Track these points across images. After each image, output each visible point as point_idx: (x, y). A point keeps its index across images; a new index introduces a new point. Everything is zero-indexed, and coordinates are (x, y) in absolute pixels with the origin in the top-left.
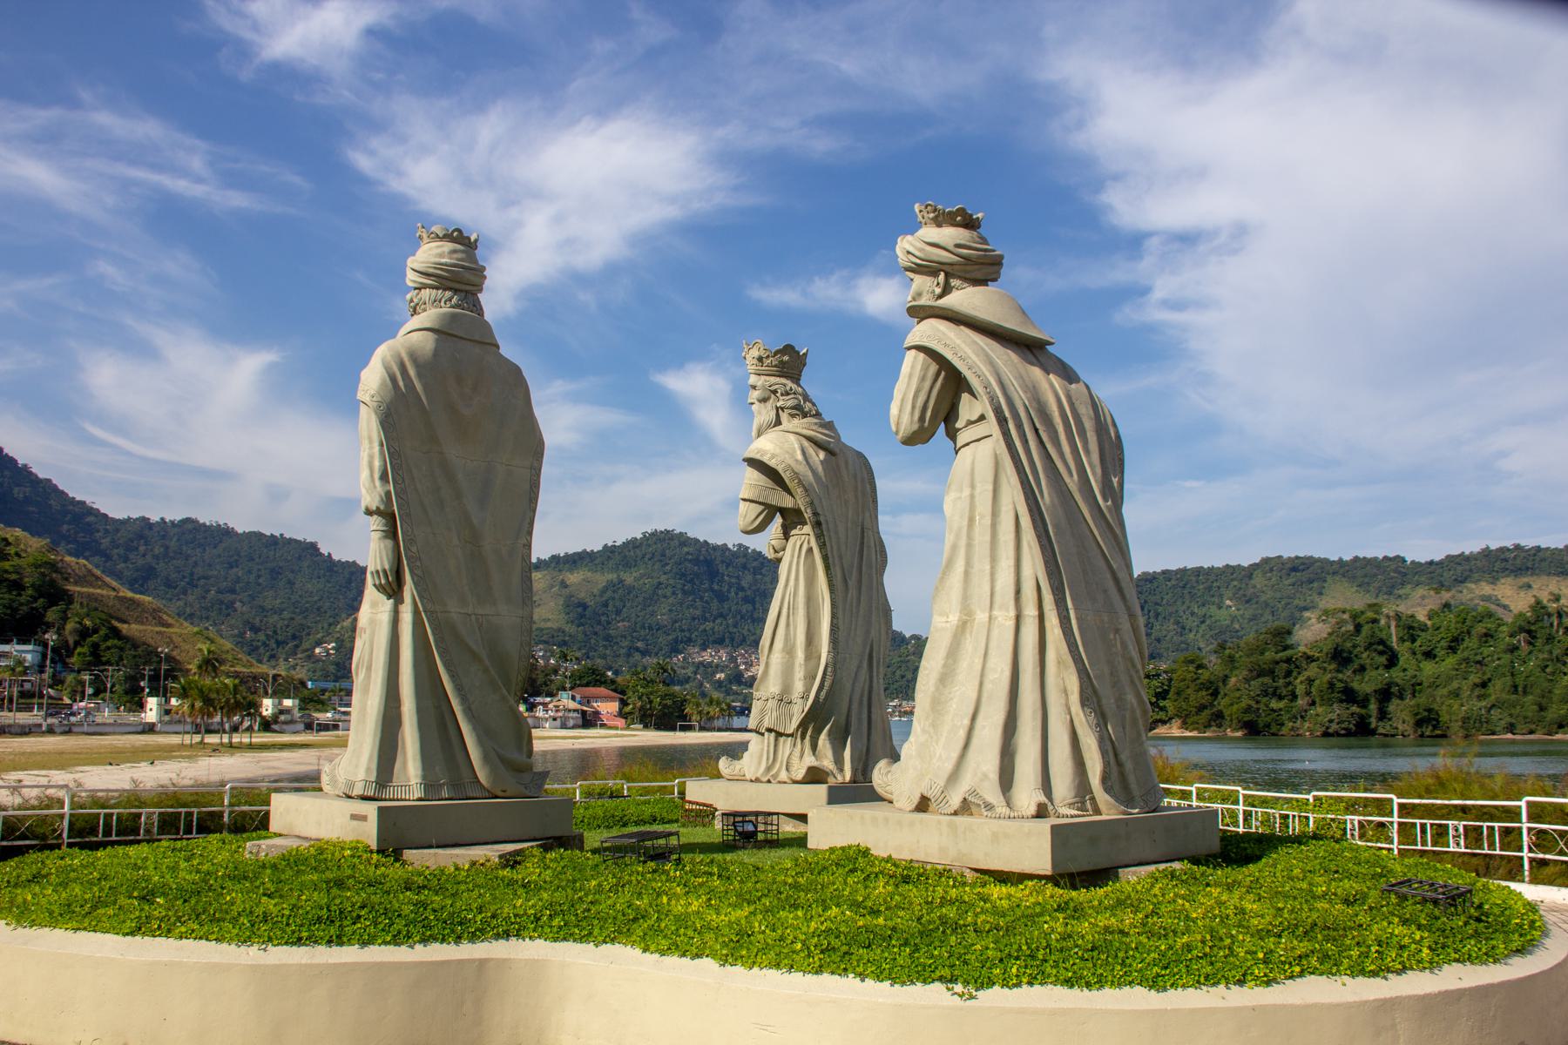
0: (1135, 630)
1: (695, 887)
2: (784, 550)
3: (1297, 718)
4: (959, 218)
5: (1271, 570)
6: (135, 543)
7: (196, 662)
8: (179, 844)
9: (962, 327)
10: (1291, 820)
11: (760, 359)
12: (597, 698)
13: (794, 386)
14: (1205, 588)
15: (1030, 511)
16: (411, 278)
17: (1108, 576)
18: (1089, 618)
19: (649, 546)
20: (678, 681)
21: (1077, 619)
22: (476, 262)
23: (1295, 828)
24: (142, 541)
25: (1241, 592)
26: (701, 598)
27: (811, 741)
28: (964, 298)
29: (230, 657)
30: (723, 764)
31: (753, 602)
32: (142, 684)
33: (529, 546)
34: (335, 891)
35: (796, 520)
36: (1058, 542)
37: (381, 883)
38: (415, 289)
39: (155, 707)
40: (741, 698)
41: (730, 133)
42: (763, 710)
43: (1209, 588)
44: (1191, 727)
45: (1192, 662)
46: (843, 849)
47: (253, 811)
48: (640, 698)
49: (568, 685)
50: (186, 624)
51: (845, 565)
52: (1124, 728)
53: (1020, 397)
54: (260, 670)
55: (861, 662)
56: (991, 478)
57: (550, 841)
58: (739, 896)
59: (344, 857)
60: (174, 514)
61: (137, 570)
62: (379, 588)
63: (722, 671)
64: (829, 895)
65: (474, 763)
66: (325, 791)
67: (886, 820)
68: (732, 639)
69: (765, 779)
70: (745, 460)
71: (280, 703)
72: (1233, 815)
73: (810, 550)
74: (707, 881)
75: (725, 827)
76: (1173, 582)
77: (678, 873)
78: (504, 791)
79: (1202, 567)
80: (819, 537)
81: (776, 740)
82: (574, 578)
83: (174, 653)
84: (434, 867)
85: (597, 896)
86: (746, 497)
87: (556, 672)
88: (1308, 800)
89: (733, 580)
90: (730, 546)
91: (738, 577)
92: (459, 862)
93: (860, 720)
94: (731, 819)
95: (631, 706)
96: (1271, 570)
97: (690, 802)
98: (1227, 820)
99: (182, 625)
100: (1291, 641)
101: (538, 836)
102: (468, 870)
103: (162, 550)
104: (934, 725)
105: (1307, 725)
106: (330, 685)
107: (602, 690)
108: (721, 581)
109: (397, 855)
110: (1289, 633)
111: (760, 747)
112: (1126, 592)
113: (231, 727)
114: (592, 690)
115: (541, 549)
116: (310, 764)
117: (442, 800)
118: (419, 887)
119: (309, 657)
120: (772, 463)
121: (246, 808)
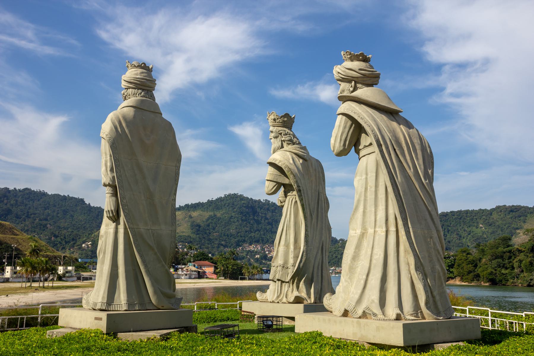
0: (439, 237)
1: (245, 350)
2: (285, 202)
3: (514, 278)
4: (361, 57)
5: (501, 211)
6: (2, 199)
7: (29, 250)
8: (16, 332)
9: (362, 105)
10: (514, 324)
11: (274, 120)
12: (205, 266)
13: (289, 131)
14: (470, 219)
15: (392, 185)
16: (124, 84)
17: (427, 213)
18: (418, 232)
19: (227, 200)
20: (240, 258)
21: (413, 232)
22: (151, 77)
23: (516, 328)
24: (6, 198)
25: (487, 221)
26: (249, 223)
27: (297, 285)
28: (363, 92)
29: (44, 249)
30: (258, 295)
31: (272, 225)
32: (4, 261)
33: (175, 200)
34: (86, 352)
35: (290, 189)
36: (405, 199)
37: (107, 348)
38: (126, 89)
39: (9, 271)
40: (266, 266)
41: (261, 23)
42: (275, 271)
43: (472, 219)
44: (465, 280)
45: (465, 252)
46: (310, 333)
47: (52, 316)
48: (223, 266)
49: (192, 260)
50: (25, 234)
51: (311, 209)
52: (435, 281)
53: (388, 135)
54: (57, 254)
55: (318, 250)
56: (374, 171)
57: (183, 329)
58: (254, 215)
59: (91, 336)
60: (20, 186)
61: (3, 211)
62: (110, 218)
63: (258, 254)
64: (304, 353)
65: (151, 297)
66: (84, 307)
67: (329, 320)
68: (263, 241)
69: (276, 301)
70: (268, 163)
71: (66, 268)
72: (486, 321)
73: (296, 202)
74: (251, 347)
75: (259, 323)
76: (456, 216)
77: (238, 343)
78: (163, 307)
79: (469, 210)
80: (300, 196)
81: (281, 284)
82: (195, 214)
83: (19, 247)
84: (131, 341)
85: (203, 353)
86: (268, 179)
87: (187, 254)
88: (522, 316)
89: (263, 215)
90: (262, 200)
91: (265, 214)
92: (142, 338)
93: (318, 276)
94: (262, 319)
95: (219, 269)
96: (501, 211)
97: (244, 311)
98: (483, 323)
99: (23, 234)
100: (511, 243)
101: (177, 327)
102: (146, 342)
103: (14, 202)
104: (350, 278)
105: (519, 281)
106: (89, 260)
107: (207, 262)
108: (258, 215)
109: (115, 335)
110: (510, 239)
111: (274, 287)
112: (435, 220)
113: (44, 279)
114: (202, 262)
115: (181, 200)
116: (79, 295)
117: (135, 310)
118: (124, 350)
119: (80, 248)
120: (280, 164)
121: (48, 315)
